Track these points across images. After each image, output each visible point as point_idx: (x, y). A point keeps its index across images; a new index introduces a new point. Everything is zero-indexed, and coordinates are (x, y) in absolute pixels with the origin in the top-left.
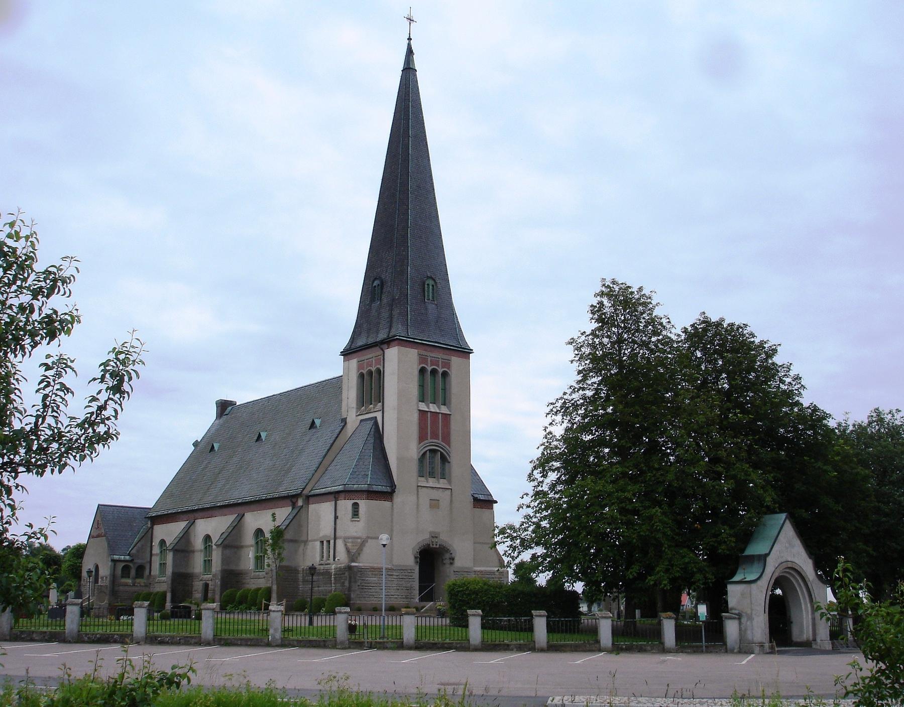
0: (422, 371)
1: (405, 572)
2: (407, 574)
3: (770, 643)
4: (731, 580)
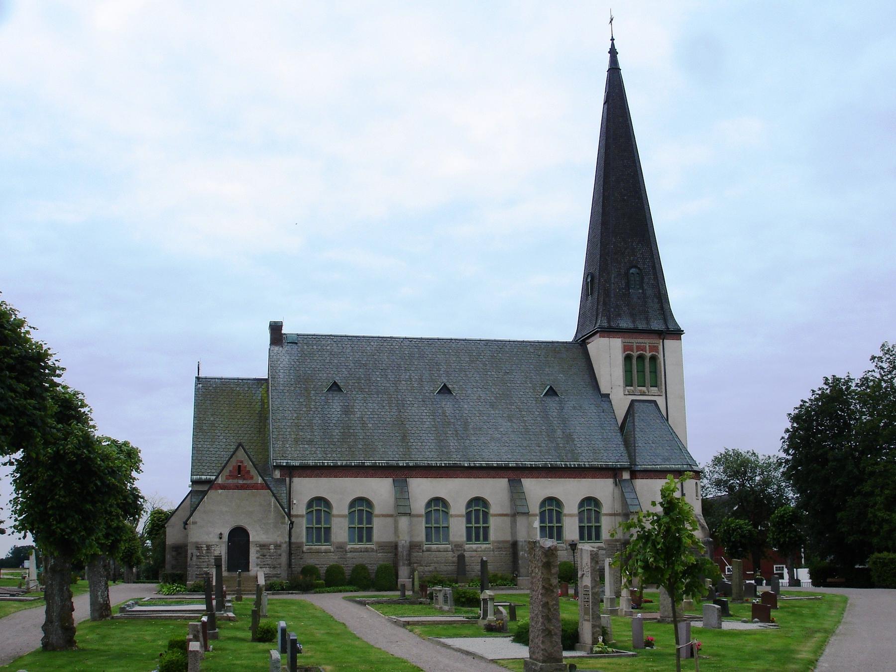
0: (628, 359)
3: (192, 522)
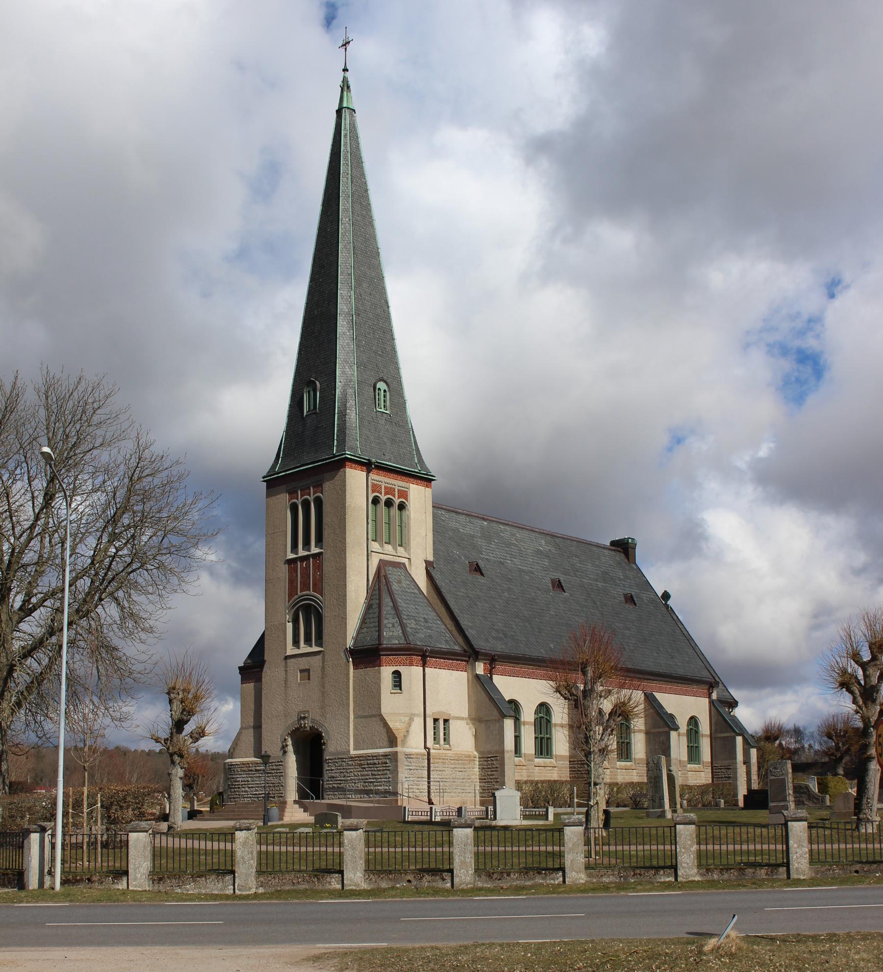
1: (272, 766)
2: (274, 767)
4: (6, 558)
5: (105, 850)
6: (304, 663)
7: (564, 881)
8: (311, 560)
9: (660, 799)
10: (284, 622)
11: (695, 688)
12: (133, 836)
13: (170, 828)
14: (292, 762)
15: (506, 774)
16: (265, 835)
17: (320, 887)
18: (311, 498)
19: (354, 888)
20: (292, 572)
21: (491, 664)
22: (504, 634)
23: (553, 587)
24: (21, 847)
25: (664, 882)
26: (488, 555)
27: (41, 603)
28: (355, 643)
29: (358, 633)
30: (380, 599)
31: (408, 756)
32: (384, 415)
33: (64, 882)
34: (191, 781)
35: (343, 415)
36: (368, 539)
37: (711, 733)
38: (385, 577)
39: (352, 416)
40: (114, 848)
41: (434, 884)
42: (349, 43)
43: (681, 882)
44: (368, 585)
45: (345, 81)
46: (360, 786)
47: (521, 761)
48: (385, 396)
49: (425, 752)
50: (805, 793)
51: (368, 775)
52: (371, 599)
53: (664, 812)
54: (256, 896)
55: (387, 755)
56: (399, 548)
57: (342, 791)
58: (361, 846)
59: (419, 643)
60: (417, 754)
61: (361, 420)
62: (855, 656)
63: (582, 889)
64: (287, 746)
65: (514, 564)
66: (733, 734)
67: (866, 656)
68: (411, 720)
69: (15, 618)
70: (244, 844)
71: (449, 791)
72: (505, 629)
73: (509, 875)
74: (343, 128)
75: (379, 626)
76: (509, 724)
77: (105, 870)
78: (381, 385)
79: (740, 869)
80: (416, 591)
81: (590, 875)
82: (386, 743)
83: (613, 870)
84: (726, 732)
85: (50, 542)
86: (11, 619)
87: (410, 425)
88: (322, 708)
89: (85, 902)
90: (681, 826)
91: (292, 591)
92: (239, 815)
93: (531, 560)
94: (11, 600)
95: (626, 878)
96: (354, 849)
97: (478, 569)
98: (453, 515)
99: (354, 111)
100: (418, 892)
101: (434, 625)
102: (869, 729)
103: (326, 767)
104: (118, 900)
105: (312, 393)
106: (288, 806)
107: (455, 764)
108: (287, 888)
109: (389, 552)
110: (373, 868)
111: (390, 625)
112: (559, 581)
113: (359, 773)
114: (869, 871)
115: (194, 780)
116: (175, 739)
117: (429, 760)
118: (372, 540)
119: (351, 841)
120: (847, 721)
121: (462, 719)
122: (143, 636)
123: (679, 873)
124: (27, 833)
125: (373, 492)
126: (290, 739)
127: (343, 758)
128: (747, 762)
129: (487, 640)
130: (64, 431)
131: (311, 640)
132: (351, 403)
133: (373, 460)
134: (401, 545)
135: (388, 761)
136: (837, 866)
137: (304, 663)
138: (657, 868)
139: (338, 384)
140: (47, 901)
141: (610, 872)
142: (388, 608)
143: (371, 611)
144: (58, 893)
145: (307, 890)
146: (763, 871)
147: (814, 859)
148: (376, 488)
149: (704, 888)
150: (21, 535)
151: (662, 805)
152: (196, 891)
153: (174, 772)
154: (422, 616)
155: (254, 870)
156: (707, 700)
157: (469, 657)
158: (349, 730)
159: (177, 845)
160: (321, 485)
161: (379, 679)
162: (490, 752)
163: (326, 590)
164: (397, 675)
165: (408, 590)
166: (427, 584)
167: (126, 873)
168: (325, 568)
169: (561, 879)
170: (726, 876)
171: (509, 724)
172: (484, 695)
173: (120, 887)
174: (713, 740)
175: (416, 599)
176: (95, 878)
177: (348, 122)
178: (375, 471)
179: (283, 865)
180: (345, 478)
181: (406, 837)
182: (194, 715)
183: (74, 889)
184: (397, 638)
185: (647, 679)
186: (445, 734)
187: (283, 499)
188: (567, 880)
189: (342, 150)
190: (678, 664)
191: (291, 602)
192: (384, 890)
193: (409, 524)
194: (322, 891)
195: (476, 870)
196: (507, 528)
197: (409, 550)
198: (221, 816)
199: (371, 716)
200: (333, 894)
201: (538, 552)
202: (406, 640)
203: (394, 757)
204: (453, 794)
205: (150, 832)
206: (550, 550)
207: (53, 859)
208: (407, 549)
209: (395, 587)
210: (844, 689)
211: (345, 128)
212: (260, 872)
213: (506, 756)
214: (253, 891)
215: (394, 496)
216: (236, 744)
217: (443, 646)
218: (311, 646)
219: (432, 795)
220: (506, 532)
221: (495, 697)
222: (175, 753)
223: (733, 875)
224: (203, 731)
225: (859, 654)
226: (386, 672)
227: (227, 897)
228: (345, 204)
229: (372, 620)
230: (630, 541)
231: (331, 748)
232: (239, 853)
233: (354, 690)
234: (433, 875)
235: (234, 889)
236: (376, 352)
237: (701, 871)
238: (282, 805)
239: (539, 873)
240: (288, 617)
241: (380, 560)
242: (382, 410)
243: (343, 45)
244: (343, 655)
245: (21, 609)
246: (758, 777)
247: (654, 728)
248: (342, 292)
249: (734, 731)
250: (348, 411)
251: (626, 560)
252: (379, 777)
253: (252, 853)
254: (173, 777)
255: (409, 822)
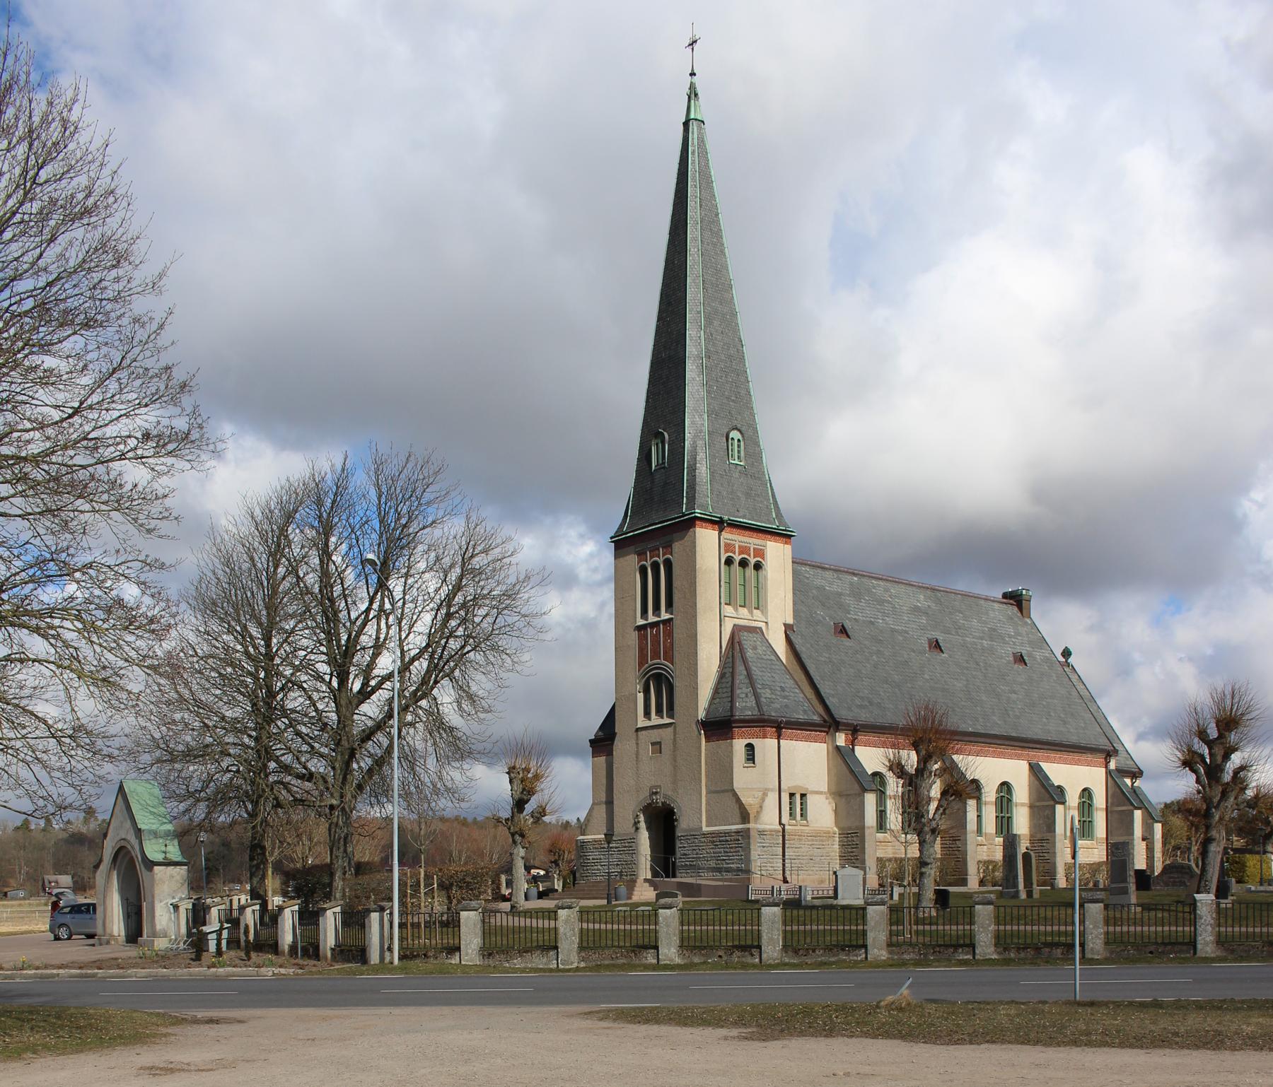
5: (445, 929)
6: (655, 735)
7: (866, 958)
8: (661, 626)
9: (1014, 879)
10: (634, 692)
11: (1089, 757)
12: (464, 914)
13: (513, 907)
14: (644, 838)
15: (866, 851)
16: (1037, 908)
17: (637, 962)
18: (661, 560)
19: (668, 962)
20: (642, 638)
21: (853, 735)
22: (869, 702)
23: (930, 647)
24: (363, 926)
25: (963, 960)
26: (857, 614)
27: (379, 686)
28: (707, 714)
29: (711, 704)
30: (733, 668)
31: (762, 833)
32: (739, 467)
33: (402, 958)
34: (556, 857)
35: (693, 469)
36: (720, 603)
37: (1107, 806)
38: (739, 643)
39: (703, 471)
40: (453, 927)
41: (744, 959)
42: (696, 41)
43: (979, 960)
44: (721, 652)
45: (692, 87)
46: (712, 864)
47: (885, 837)
48: (739, 446)
49: (780, 828)
50: (1187, 873)
51: (720, 853)
52: (724, 668)
53: (1017, 892)
54: (577, 969)
55: (739, 832)
56: (755, 611)
57: (694, 868)
58: (675, 923)
59: (773, 714)
60: (771, 831)
61: (712, 474)
62: (1202, 734)
63: (878, 965)
64: (639, 822)
65: (886, 624)
66: (1131, 808)
67: (1213, 733)
68: (765, 795)
69: (355, 702)
70: (567, 921)
71: (805, 868)
72: (871, 696)
73: (814, 951)
74: (690, 144)
75: (732, 696)
76: (870, 799)
77: (439, 946)
78: (735, 435)
79: (1037, 948)
80: (773, 658)
81: (890, 953)
82: (738, 819)
83: (914, 948)
84: (1124, 805)
85: (387, 623)
86: (350, 702)
87: (767, 476)
88: (675, 782)
89: (419, 974)
90: (980, 906)
91: (642, 660)
92: (588, 894)
93: (906, 618)
94: (350, 681)
95: (925, 955)
96: (668, 926)
97: (843, 631)
98: (819, 571)
99: (703, 122)
100: (727, 966)
101: (791, 694)
102: (1210, 809)
103: (678, 844)
104: (448, 973)
105: (660, 445)
106: (637, 885)
107: (813, 840)
108: (606, 962)
109: (744, 616)
110: (686, 944)
111: (744, 695)
112: (937, 641)
113: (712, 851)
114: (1163, 952)
115: (559, 856)
116: (516, 819)
117: (784, 836)
118: (726, 604)
119: (665, 919)
120: (1192, 801)
121: (821, 793)
122: (482, 716)
123: (977, 951)
124: (368, 911)
125: (726, 551)
126: (642, 815)
127: (696, 834)
128: (1148, 838)
129: (849, 709)
130: (396, 510)
131: (662, 711)
132: (701, 456)
133: (726, 518)
134: (757, 608)
135: (740, 838)
136: (1132, 947)
137: (655, 735)
138: (956, 947)
139: (687, 435)
140: (385, 974)
141: (911, 950)
142: (742, 677)
143: (724, 680)
144: (395, 968)
145: (625, 964)
146: (1059, 951)
147: (1220, 941)
148: (729, 547)
149: (1002, 965)
150: (357, 619)
151: (1015, 885)
152: (523, 965)
153: (515, 851)
154: (778, 684)
155: (576, 946)
156: (1104, 769)
157: (829, 728)
158: (701, 806)
159: (516, 924)
160: (671, 546)
161: (731, 752)
162: (850, 828)
163: (676, 660)
164: (750, 747)
165: (764, 657)
166: (787, 649)
167: (458, 949)
168: (675, 635)
169: (864, 956)
170: (1022, 955)
171: (870, 799)
172: (845, 768)
173: (453, 962)
174: (1109, 815)
175: (773, 667)
176: (430, 954)
177: (696, 136)
178: (728, 529)
179: (609, 943)
180: (695, 538)
181: (736, 915)
182: (534, 794)
183: (411, 963)
184: (751, 709)
185: (1033, 748)
186: (802, 809)
187: (632, 560)
188: (869, 956)
189: (689, 169)
190: (1072, 730)
191: (641, 671)
192: (696, 965)
193: (766, 584)
194: (639, 966)
195: (784, 946)
196: (881, 583)
197: (767, 613)
198: (571, 895)
199: (723, 791)
200: (647, 967)
201: (916, 610)
202: (759, 711)
203: (746, 834)
204: (811, 873)
205: (480, 910)
206: (929, 606)
207: (392, 938)
208: (764, 612)
209: (750, 653)
210: (1187, 769)
211: (693, 144)
212: (582, 948)
213: (867, 832)
214: (575, 965)
215: (749, 555)
216: (588, 821)
217: (801, 717)
218: (662, 718)
219: (788, 873)
220: (879, 588)
221: (856, 770)
222: (516, 832)
223: (1031, 952)
224: (544, 810)
225: (1206, 732)
226: (739, 745)
227: (551, 970)
228: (693, 232)
229: (725, 690)
230: (1024, 592)
231: (684, 824)
232: (561, 930)
233: (706, 764)
234: (742, 951)
235: (558, 963)
236: (728, 398)
237: (998, 950)
238: (631, 885)
239: (843, 950)
240: (638, 687)
241: (734, 625)
242: (736, 462)
243: (690, 45)
244: (694, 726)
245: (359, 692)
246: (1163, 855)
247: (1038, 801)
248: (691, 332)
249: (1133, 805)
250: (698, 465)
251: (1019, 614)
252: (731, 854)
253: (573, 930)
254: (515, 857)
255: (752, 901)
